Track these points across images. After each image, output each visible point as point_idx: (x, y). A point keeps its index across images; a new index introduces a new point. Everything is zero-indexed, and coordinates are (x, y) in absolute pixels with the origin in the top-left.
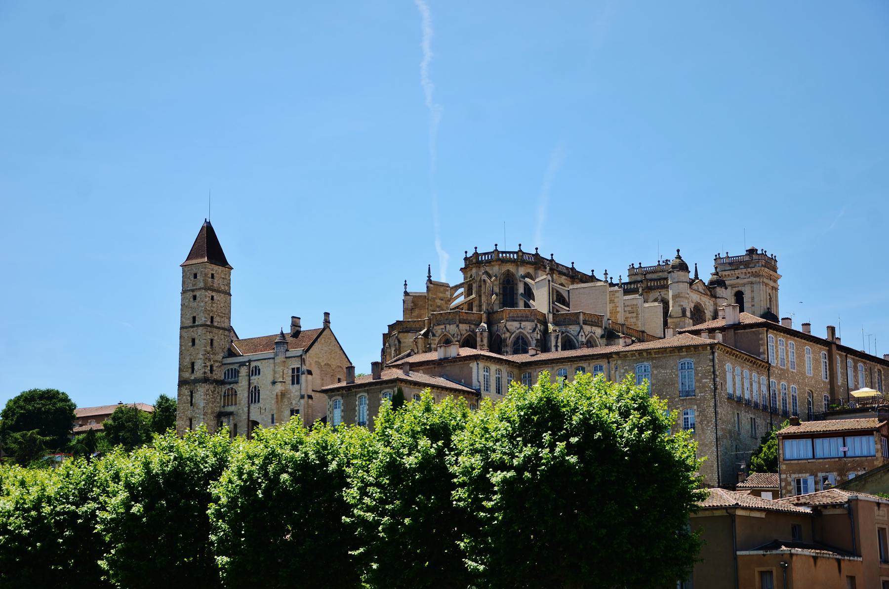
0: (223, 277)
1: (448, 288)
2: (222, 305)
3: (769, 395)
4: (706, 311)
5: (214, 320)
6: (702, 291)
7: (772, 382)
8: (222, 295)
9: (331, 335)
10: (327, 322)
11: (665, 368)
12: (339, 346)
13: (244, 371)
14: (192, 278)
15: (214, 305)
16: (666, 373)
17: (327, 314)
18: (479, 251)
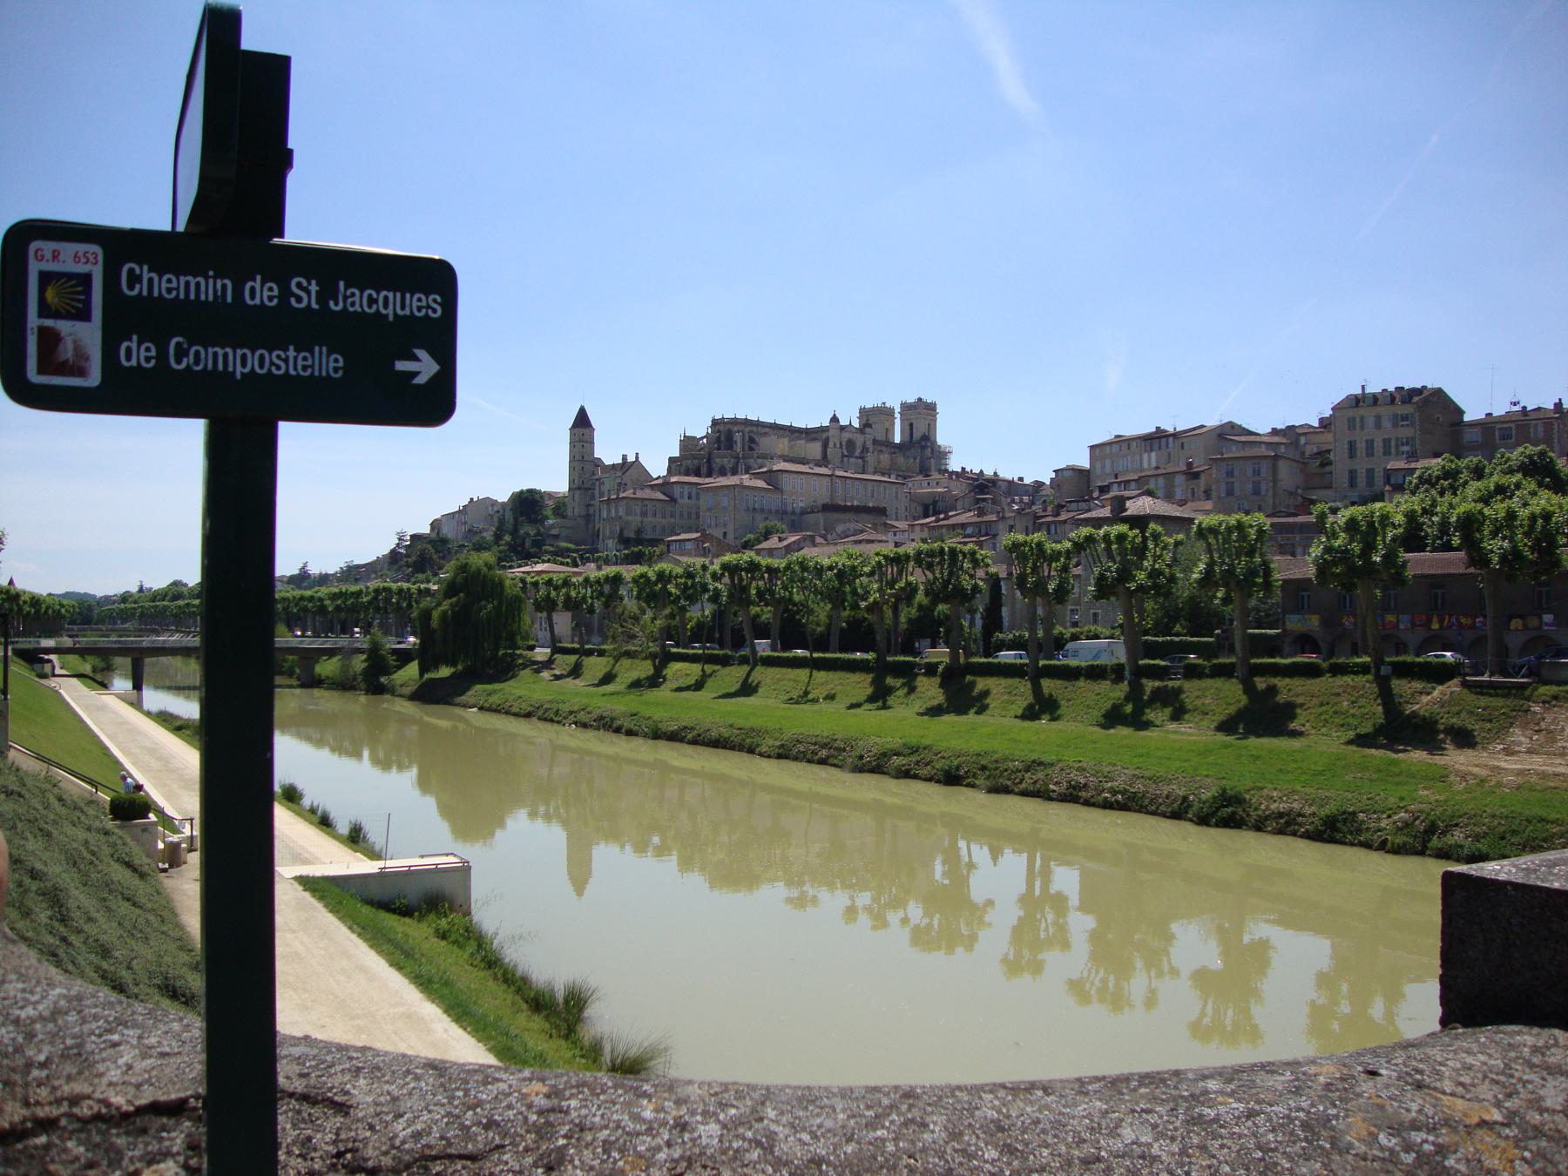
10: (637, 457)
13: (598, 483)
17: (637, 454)
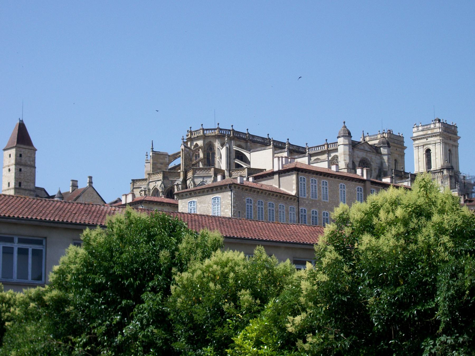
0: (29, 155)
1: (167, 156)
2: (28, 174)
3: (297, 218)
4: (372, 163)
5: (22, 184)
6: (369, 150)
7: (302, 210)
8: (29, 168)
9: (93, 191)
10: (91, 183)
11: (205, 203)
12: (100, 198)
14: (8, 156)
15: (21, 175)
16: (205, 206)
18: (193, 130)
